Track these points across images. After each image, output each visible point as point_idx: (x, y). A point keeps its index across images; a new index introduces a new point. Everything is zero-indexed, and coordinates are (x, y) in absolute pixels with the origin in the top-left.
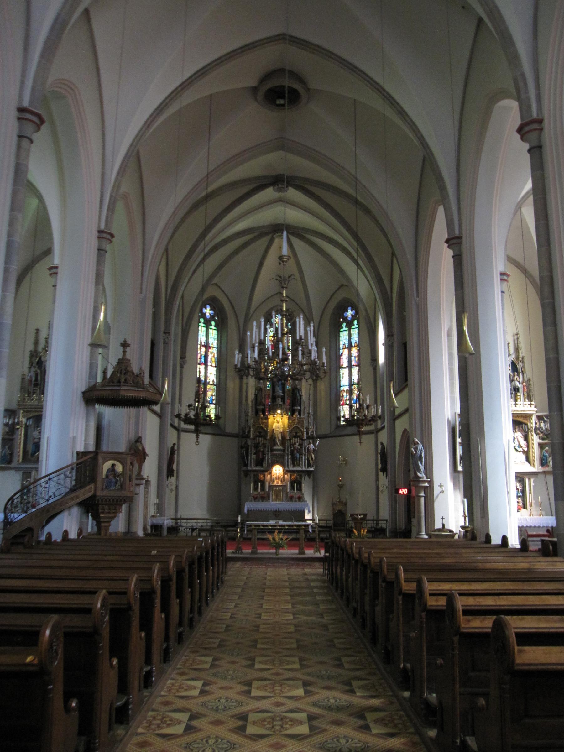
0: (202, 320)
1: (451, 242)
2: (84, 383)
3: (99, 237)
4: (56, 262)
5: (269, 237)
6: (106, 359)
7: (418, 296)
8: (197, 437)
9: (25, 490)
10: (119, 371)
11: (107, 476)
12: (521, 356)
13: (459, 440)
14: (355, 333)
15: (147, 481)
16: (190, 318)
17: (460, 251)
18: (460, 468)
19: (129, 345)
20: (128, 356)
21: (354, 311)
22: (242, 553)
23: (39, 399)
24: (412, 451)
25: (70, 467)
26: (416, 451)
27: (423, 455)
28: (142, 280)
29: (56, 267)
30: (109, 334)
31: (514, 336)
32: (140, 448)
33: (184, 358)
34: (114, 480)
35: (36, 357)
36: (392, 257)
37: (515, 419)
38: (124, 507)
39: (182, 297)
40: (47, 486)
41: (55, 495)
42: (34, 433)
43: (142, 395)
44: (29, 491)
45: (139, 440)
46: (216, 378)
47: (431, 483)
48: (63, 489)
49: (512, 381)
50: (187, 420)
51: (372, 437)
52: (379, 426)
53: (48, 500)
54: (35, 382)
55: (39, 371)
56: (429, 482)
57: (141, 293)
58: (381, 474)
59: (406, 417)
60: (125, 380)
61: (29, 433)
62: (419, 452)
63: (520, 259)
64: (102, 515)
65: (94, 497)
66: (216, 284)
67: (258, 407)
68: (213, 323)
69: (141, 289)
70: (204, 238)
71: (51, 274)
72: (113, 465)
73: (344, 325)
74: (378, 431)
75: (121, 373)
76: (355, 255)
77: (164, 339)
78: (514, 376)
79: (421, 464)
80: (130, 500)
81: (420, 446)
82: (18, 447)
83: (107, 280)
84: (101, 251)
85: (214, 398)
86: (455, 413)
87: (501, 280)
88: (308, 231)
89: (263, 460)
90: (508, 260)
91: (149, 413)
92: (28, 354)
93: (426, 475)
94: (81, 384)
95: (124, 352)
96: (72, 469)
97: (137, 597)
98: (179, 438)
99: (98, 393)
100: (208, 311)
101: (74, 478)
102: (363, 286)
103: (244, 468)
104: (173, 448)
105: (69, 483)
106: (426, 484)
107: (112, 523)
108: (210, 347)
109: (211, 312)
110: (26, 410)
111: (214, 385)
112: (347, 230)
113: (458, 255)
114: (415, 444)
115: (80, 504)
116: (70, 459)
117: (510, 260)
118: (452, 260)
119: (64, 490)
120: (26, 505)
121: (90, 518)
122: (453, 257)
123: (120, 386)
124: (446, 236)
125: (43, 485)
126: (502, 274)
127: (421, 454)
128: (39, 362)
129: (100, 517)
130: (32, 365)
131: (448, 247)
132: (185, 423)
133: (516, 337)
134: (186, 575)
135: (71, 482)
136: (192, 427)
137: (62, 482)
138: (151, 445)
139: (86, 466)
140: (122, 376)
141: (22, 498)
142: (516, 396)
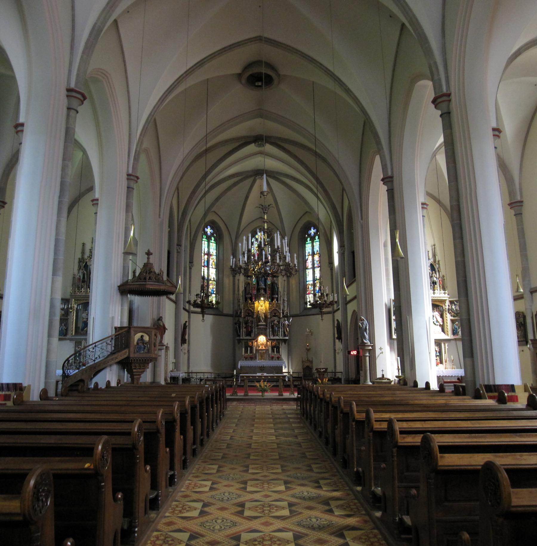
0: (204, 237)
1: (386, 180)
4: (97, 196)
5: (252, 179)
7: (362, 219)
8: (203, 317)
9: (77, 354)
11: (138, 344)
12: (437, 260)
13: (393, 317)
18: (394, 337)
19: (152, 254)
20: (151, 261)
22: (237, 395)
27: (367, 328)
29: (97, 200)
31: (432, 246)
32: (161, 324)
34: (143, 346)
38: (150, 365)
39: (190, 220)
43: (162, 288)
45: (160, 319)
47: (374, 347)
49: (431, 277)
50: (195, 305)
51: (330, 316)
52: (335, 308)
53: (94, 361)
56: (372, 346)
57: (160, 217)
58: (337, 341)
60: (150, 278)
61: (79, 314)
62: (364, 326)
63: (436, 195)
64: (134, 370)
65: (128, 358)
68: (213, 238)
69: (160, 215)
72: (142, 336)
73: (309, 239)
74: (334, 312)
80: (154, 360)
84: (129, 189)
85: (214, 290)
89: (251, 331)
91: (167, 300)
95: (148, 258)
96: (112, 339)
98: (189, 317)
100: (209, 230)
101: (113, 345)
102: (322, 212)
103: (238, 338)
104: (185, 324)
105: (110, 349)
106: (370, 348)
107: (142, 375)
108: (211, 255)
109: (212, 231)
116: (110, 332)
117: (428, 194)
121: (126, 372)
123: (145, 282)
124: (382, 177)
126: (423, 204)
127: (366, 327)
129: (133, 372)
136: (199, 310)
137: (105, 348)
138: (169, 322)
139: (122, 337)
141: (75, 359)
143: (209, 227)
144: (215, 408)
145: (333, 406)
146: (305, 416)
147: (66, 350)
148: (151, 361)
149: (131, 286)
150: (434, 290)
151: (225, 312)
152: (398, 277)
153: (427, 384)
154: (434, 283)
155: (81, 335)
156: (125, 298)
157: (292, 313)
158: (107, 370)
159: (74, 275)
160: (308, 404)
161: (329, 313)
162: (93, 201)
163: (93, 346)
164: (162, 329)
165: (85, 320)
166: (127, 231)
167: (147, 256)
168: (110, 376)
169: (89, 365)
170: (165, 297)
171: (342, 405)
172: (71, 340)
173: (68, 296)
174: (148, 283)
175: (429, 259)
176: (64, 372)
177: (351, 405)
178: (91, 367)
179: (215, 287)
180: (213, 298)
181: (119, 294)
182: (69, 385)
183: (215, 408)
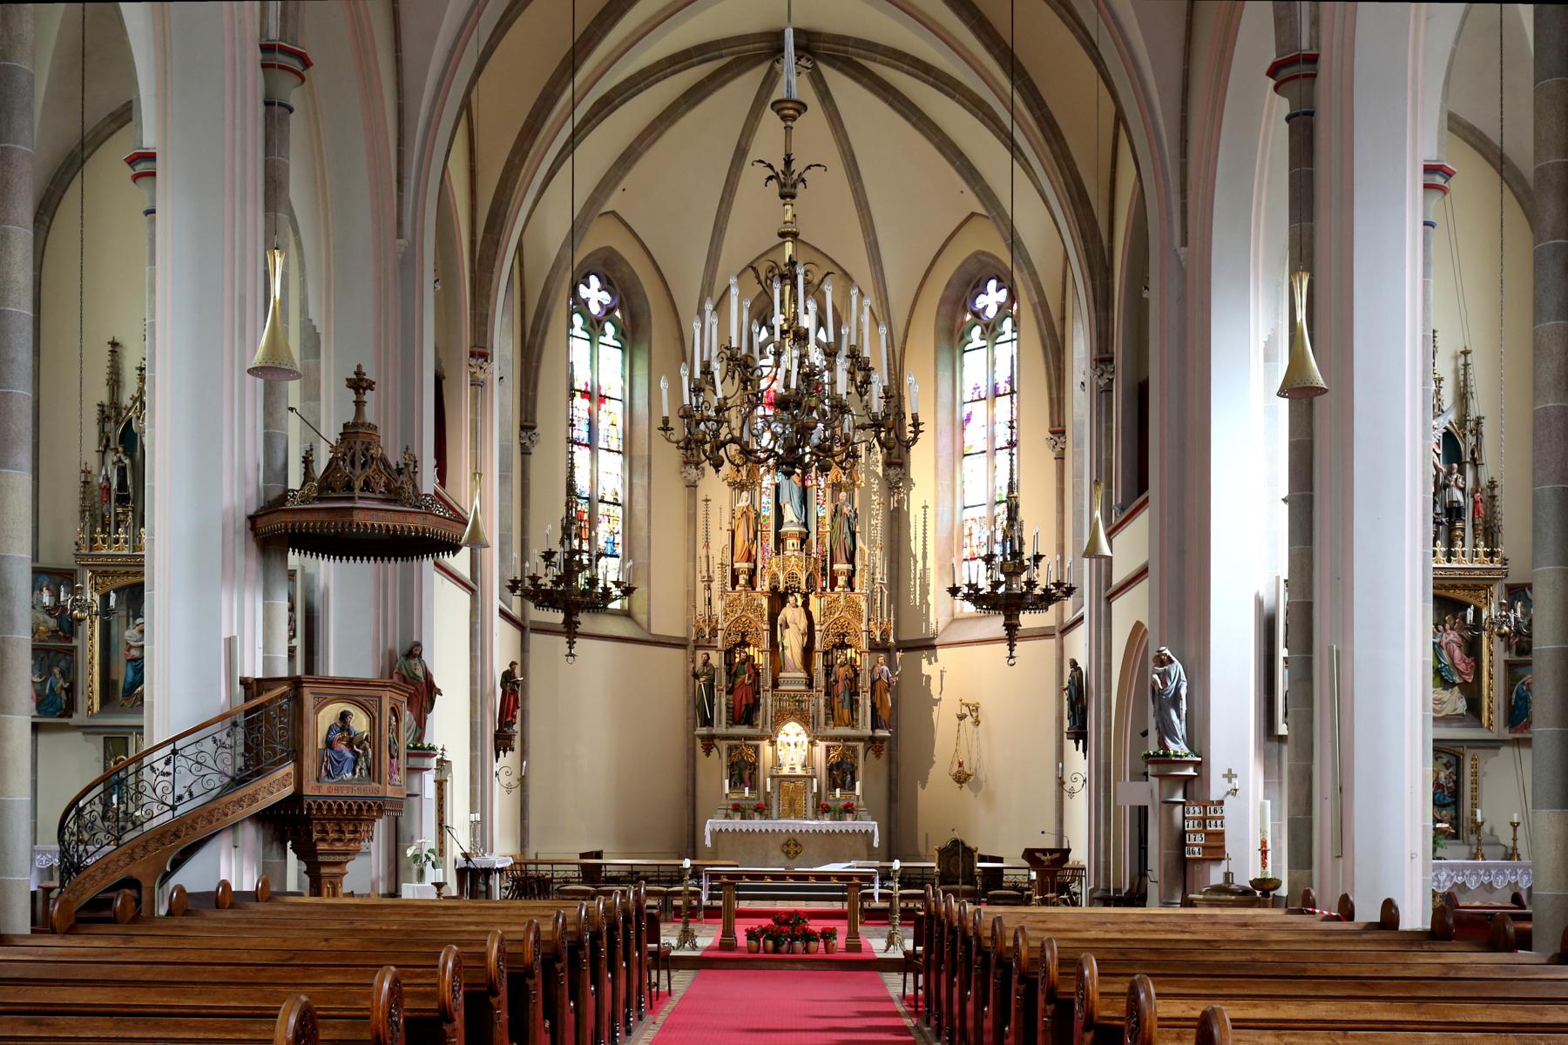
0: (578, 319)
1: (1285, 73)
2: (251, 491)
3: (264, 66)
4: (149, 141)
5: (763, 69)
6: (311, 425)
7: (1184, 243)
8: (571, 644)
9: (112, 781)
10: (348, 458)
11: (329, 744)
12: (1473, 415)
13: (1282, 652)
14: (1005, 352)
15: (441, 762)
16: (543, 313)
17: (1310, 97)
18: (1282, 729)
19: (371, 386)
20: (370, 416)
21: (1004, 292)
22: (694, 947)
23: (137, 543)
24: (1155, 682)
25: (228, 721)
26: (1164, 683)
27: (1183, 692)
28: (400, 198)
29: (151, 157)
30: (318, 355)
31: (1456, 358)
32: (420, 673)
33: (534, 428)
34: (349, 755)
35: (117, 423)
36: (1116, 128)
37: (1443, 592)
38: (380, 827)
39: (520, 247)
40: (169, 769)
41: (191, 794)
42: (127, 633)
43: (414, 523)
44: (121, 782)
45: (414, 652)
46: (623, 485)
47: (1202, 766)
48: (215, 777)
49: (1440, 487)
50: (545, 598)
51: (1050, 644)
52: (1069, 617)
53: (173, 808)
54: (119, 498)
55: (127, 461)
56: (1197, 765)
57: (400, 236)
58: (1070, 744)
59: (1141, 589)
60: (367, 483)
61: (114, 630)
62: (1172, 686)
63: (1488, 126)
64: (322, 846)
65: (297, 797)
66: (613, 213)
67: (737, 565)
68: (610, 328)
69: (400, 224)
70: (573, 76)
71: (136, 178)
72: (344, 716)
73: (977, 331)
74: (1066, 629)
75: (353, 464)
76: (1005, 117)
77: (472, 374)
78: (1450, 473)
79: (1179, 716)
80: (396, 811)
81: (1176, 668)
82: (84, 669)
83: (297, 192)
84: (275, 109)
85: (619, 539)
86: (1278, 578)
87: (1426, 186)
88: (873, 48)
89: (754, 706)
90: (1450, 129)
91: (438, 578)
92: (93, 415)
93: (1190, 744)
94: (237, 493)
95: (359, 404)
96: (235, 724)
97: (397, 1024)
98: (524, 648)
99: (288, 518)
100: (595, 295)
101: (241, 749)
102: (1039, 223)
103: (703, 731)
104: (508, 677)
105: (230, 762)
106: (1190, 771)
107: (349, 867)
108: (603, 398)
109: (605, 297)
110: (100, 569)
111: (616, 504)
112: (988, 48)
113: (1305, 114)
114: (1162, 664)
115: (261, 818)
116: (222, 698)
117: (1456, 125)
118: (1285, 127)
119: (215, 781)
120: (119, 822)
121: (291, 856)
122: (1288, 119)
123: (351, 499)
124: (1272, 57)
125: (160, 765)
126: (1429, 169)
127: (1178, 689)
128: (123, 435)
129: (315, 853)
130: (107, 446)
131: (1276, 88)
132: (538, 605)
133: (1461, 361)
134: (536, 987)
135: (234, 758)
136: (558, 617)
137: (210, 762)
138: (448, 662)
139: (266, 718)
140: (358, 470)
141: (106, 804)
142: (1451, 528)
143: (593, 280)
144: (608, 988)
145: (1052, 996)
146: (933, 1022)
147: (75, 764)
148: (381, 810)
149: (298, 518)
150: (1450, 543)
151: (659, 628)
152: (1310, 487)
153: (1389, 907)
154: (1453, 513)
155: (122, 710)
156: (275, 561)
157: (906, 636)
158: (221, 845)
159: (87, 472)
160: (943, 977)
161: (1044, 634)
162: (133, 160)
163: (167, 750)
164: (423, 694)
165: (134, 653)
166: (895, 702)
167: (352, 395)
168: (231, 865)
169: (155, 823)
170: (428, 563)
171: (1054, 969)
172: (87, 730)
173: (67, 561)
174: (360, 504)
175: (1439, 411)
176: (64, 853)
177: (1079, 965)
178: (163, 833)
179: (619, 527)
180: (609, 571)
181: (253, 546)
182: (86, 897)
183: (608, 988)
